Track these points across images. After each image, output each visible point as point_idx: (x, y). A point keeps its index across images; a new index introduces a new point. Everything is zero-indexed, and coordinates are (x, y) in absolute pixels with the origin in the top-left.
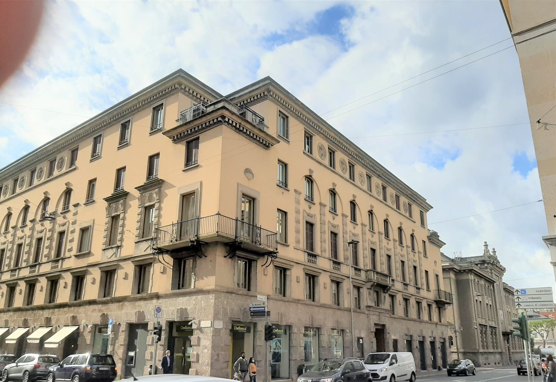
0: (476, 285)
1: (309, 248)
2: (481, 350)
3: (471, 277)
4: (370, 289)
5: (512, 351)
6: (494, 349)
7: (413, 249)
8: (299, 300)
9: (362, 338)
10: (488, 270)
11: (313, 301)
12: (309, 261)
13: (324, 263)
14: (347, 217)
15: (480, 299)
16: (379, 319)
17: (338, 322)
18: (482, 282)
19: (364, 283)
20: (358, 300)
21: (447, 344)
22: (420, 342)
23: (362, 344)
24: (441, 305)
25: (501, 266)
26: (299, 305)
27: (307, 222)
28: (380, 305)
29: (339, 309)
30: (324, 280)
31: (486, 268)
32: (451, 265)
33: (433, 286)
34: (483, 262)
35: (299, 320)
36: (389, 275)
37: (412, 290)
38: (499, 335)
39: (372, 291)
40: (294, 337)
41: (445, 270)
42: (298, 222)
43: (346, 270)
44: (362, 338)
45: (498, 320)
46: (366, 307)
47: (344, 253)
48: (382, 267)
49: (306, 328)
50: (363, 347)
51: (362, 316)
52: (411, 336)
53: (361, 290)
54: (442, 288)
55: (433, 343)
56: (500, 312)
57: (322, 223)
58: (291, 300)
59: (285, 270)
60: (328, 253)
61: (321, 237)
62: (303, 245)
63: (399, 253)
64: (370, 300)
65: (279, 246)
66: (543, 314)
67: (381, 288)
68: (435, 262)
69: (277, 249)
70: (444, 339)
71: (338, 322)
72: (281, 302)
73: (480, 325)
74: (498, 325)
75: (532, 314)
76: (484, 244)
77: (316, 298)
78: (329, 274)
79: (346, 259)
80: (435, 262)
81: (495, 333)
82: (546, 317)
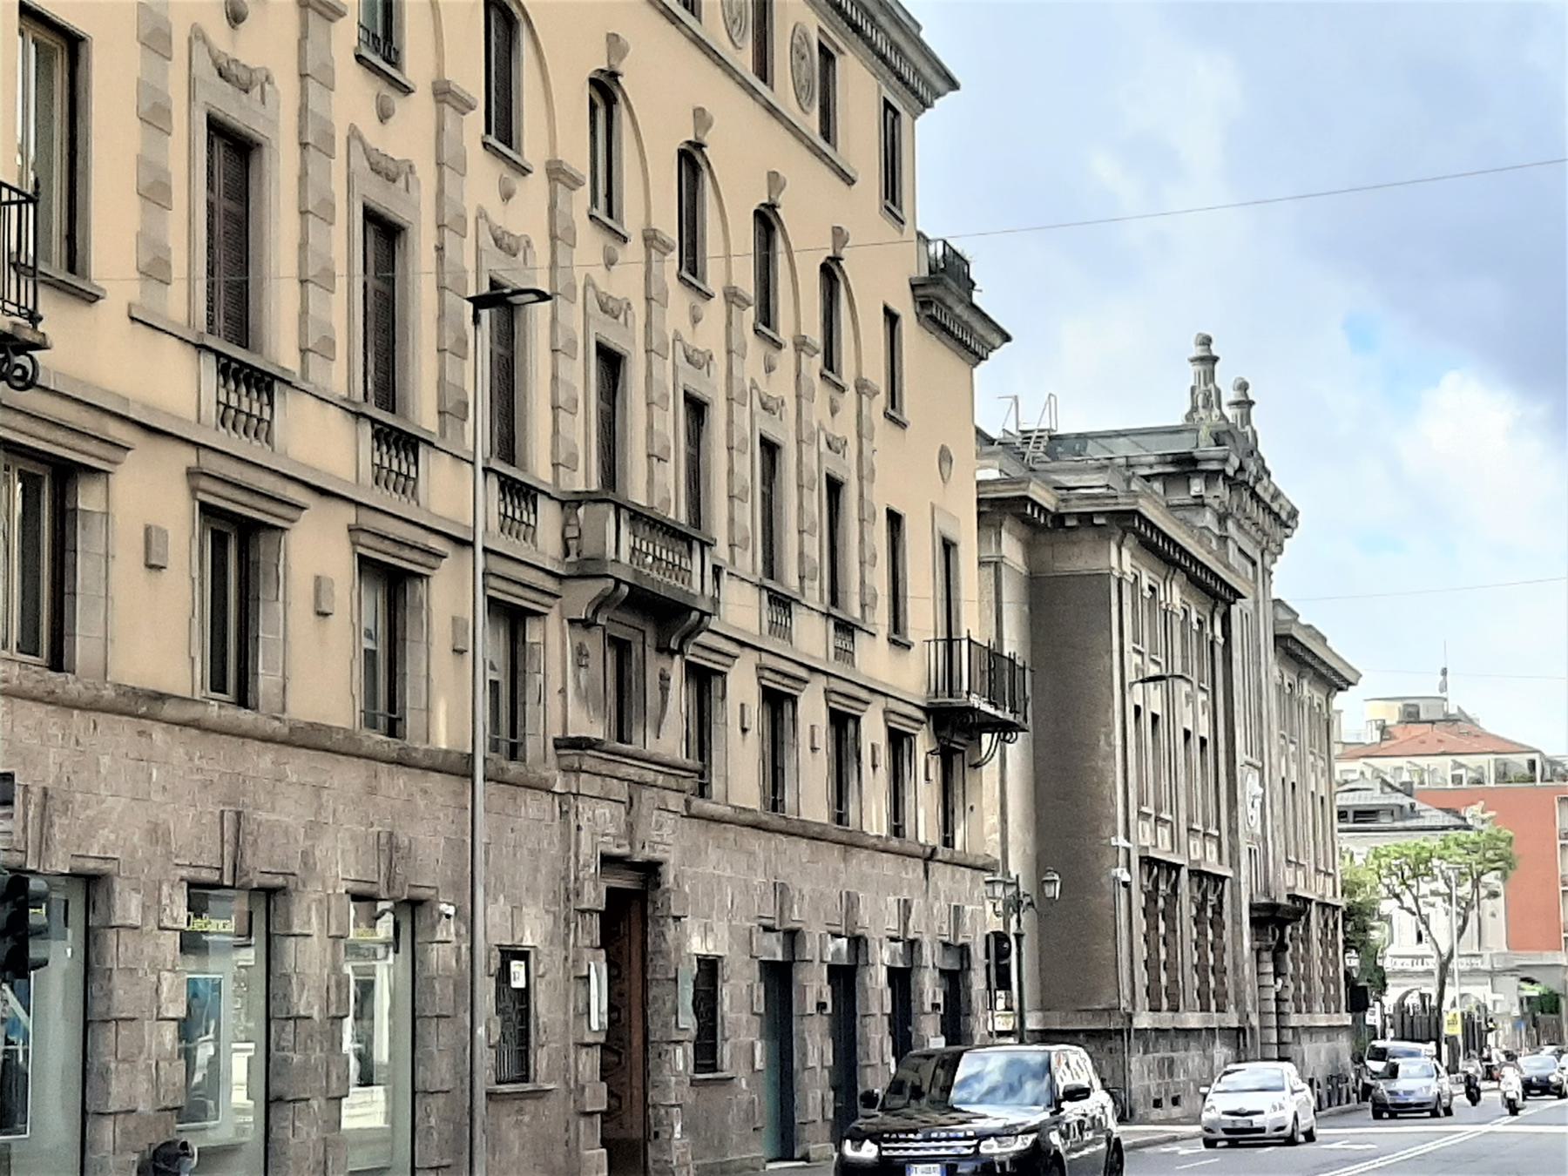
0: (1143, 608)
1: (220, 323)
2: (1143, 1020)
3: (1122, 560)
4: (587, 624)
5: (1294, 1020)
6: (1205, 1008)
7: (830, 362)
8: (160, 697)
9: (523, 956)
10: (1208, 519)
11: (242, 701)
12: (227, 416)
13: (317, 439)
14: (466, 106)
15: (1155, 704)
16: (631, 827)
17: (391, 849)
18: (1175, 595)
19: (550, 584)
20: (510, 698)
21: (978, 981)
22: (891, 971)
23: (524, 994)
24: (956, 729)
25: (1277, 495)
26: (158, 733)
27: (217, 129)
28: (637, 737)
29: (402, 762)
30: (315, 556)
31: (1200, 503)
32: (1009, 481)
33: (923, 619)
34: (1185, 466)
35: (156, 834)
36: (688, 537)
37: (810, 636)
38: (1237, 921)
39: (594, 642)
40: (118, 951)
41: (996, 510)
42: (155, 117)
43: (452, 491)
44: (523, 956)
45: (1233, 831)
46: (558, 744)
47: (443, 367)
48: (654, 483)
49: (200, 895)
50: (525, 1014)
51: (534, 807)
52: (792, 937)
53: (533, 632)
54: (974, 623)
55: (844, 978)
56: (1250, 785)
57: (313, 142)
58: (109, 693)
59: (66, 474)
60: (342, 373)
61: (303, 246)
62: (185, 298)
63: (759, 386)
64: (584, 697)
65: (47, 304)
66: (1432, 796)
67: (657, 617)
68: (945, 456)
69: (34, 318)
70: (964, 951)
71: (391, 849)
72: (39, 711)
73: (1148, 862)
74: (1234, 863)
75: (1372, 798)
76: (1197, 351)
77: (266, 681)
78: (349, 515)
79: (450, 411)
80: (945, 456)
81: (1218, 909)
82: (1449, 820)
